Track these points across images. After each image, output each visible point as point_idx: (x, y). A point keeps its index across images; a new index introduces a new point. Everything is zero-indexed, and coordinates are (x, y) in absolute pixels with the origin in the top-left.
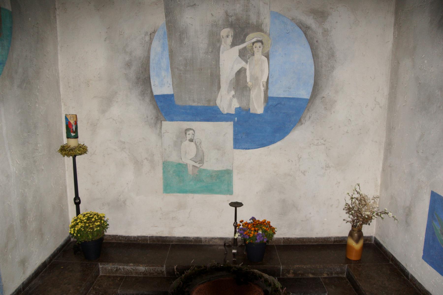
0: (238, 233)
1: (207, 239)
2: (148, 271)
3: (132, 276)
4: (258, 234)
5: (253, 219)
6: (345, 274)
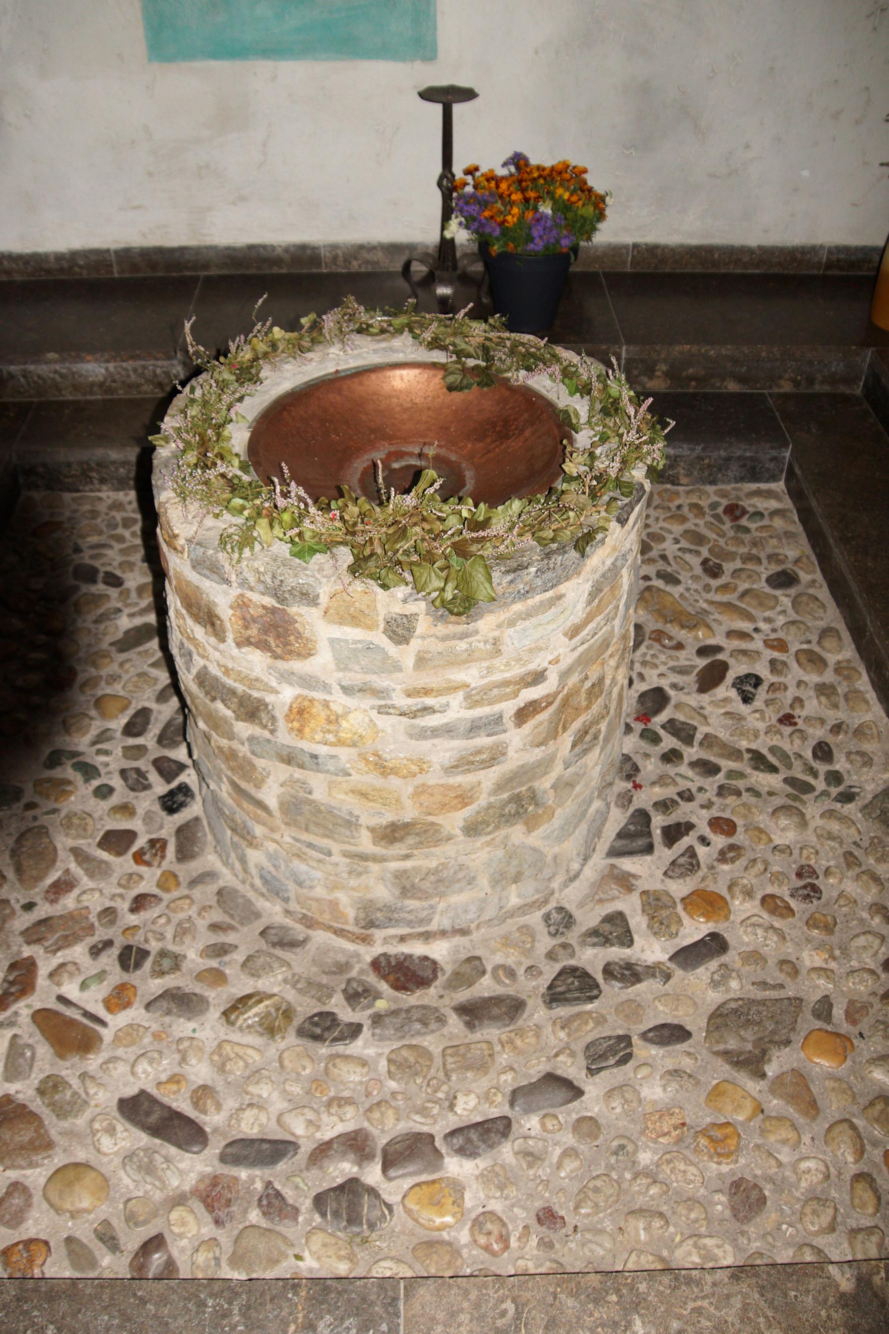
0: (457, 217)
1: (339, 252)
2: (117, 377)
3: (61, 398)
4: (539, 219)
5: (518, 161)
6: (862, 384)
